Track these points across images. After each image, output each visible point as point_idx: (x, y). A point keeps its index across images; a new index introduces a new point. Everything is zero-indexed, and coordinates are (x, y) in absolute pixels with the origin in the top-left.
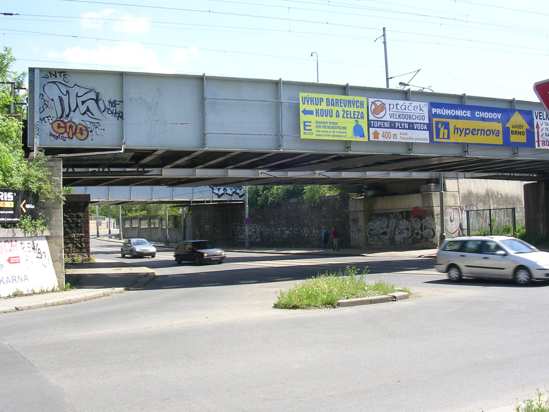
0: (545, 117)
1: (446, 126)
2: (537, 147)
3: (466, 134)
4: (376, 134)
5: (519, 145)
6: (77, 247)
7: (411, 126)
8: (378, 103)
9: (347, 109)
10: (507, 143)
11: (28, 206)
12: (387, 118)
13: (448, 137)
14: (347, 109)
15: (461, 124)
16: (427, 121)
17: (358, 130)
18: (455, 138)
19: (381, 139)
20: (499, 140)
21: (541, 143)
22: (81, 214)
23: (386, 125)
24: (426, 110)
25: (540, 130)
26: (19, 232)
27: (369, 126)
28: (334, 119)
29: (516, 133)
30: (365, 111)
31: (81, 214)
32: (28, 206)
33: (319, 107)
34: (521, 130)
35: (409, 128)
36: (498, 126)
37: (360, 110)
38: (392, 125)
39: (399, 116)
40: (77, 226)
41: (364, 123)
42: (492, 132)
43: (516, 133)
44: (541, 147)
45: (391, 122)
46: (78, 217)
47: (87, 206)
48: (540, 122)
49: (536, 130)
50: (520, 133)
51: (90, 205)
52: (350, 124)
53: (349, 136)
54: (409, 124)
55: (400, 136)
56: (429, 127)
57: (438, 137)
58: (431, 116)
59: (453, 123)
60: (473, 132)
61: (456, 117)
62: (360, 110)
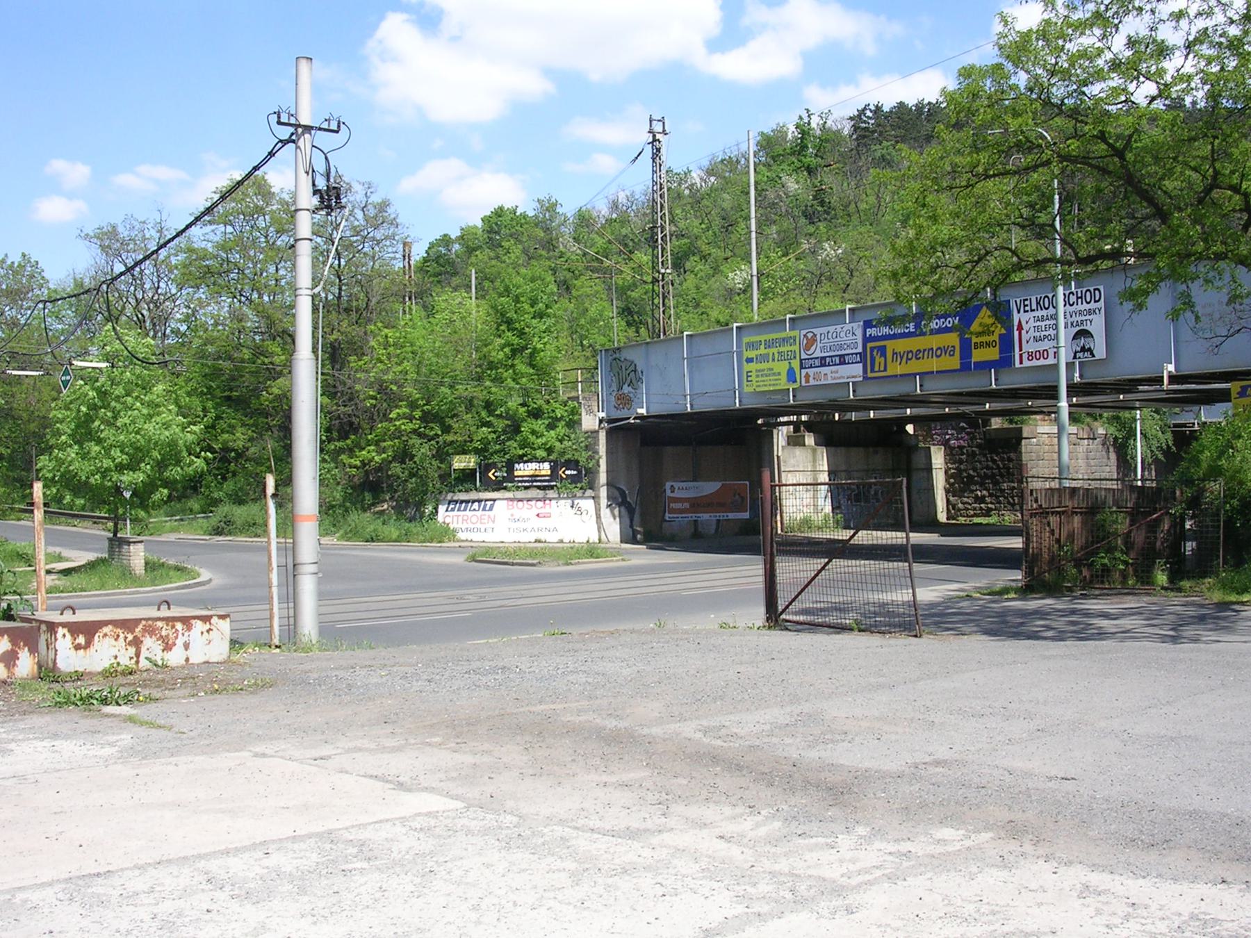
0: (1034, 307)
1: (882, 350)
2: (1017, 365)
3: (908, 359)
4: (807, 376)
5: (985, 366)
6: (1009, 503)
7: (842, 360)
8: (810, 335)
9: (781, 349)
10: (965, 367)
11: (568, 472)
12: (818, 354)
13: (885, 370)
14: (781, 349)
15: (901, 345)
16: (860, 350)
17: (791, 376)
18: (897, 369)
19: (812, 382)
20: (954, 362)
21: (1025, 356)
22: (1012, 455)
23: (817, 363)
24: (859, 333)
25: (1023, 332)
26: (551, 494)
27: (802, 367)
28: (770, 365)
29: (982, 345)
30: (796, 348)
31: (1012, 455)
32: (568, 472)
33: (758, 352)
34: (991, 338)
35: (841, 364)
36: (953, 339)
37: (792, 348)
38: (823, 362)
39: (1038, 303)
40: (1008, 473)
41: (796, 364)
42: (944, 350)
43: (982, 345)
44: (1026, 363)
45: (824, 358)
46: (1010, 460)
47: (1019, 443)
48: (1024, 317)
49: (1016, 333)
50: (988, 344)
51: (1023, 442)
52: (783, 367)
53: (783, 383)
54: (840, 356)
55: (830, 375)
56: (863, 359)
57: (872, 371)
58: (866, 340)
59: (890, 345)
60: (917, 355)
61: (894, 337)
62: (792, 348)
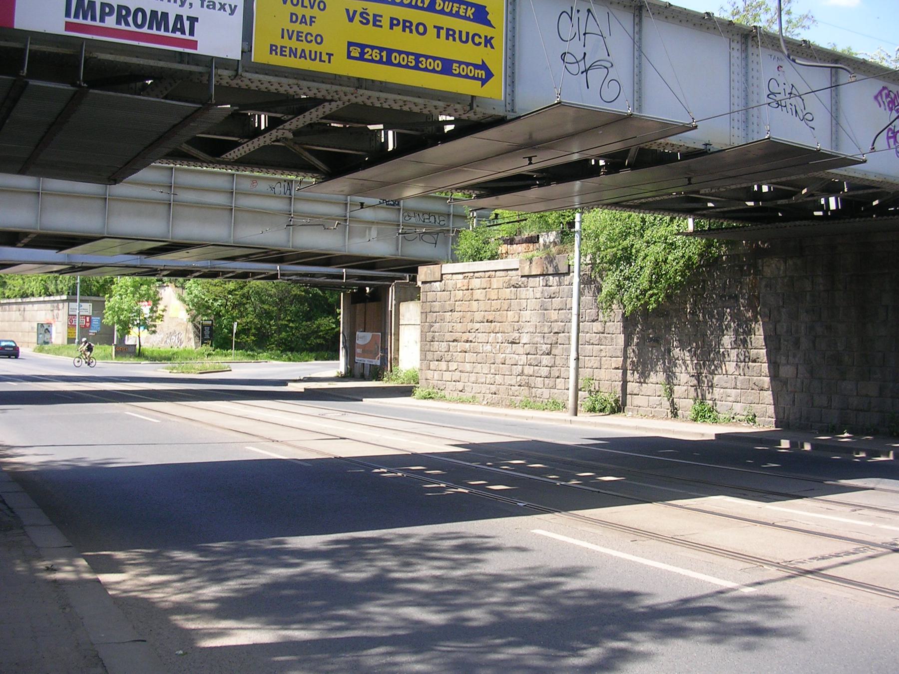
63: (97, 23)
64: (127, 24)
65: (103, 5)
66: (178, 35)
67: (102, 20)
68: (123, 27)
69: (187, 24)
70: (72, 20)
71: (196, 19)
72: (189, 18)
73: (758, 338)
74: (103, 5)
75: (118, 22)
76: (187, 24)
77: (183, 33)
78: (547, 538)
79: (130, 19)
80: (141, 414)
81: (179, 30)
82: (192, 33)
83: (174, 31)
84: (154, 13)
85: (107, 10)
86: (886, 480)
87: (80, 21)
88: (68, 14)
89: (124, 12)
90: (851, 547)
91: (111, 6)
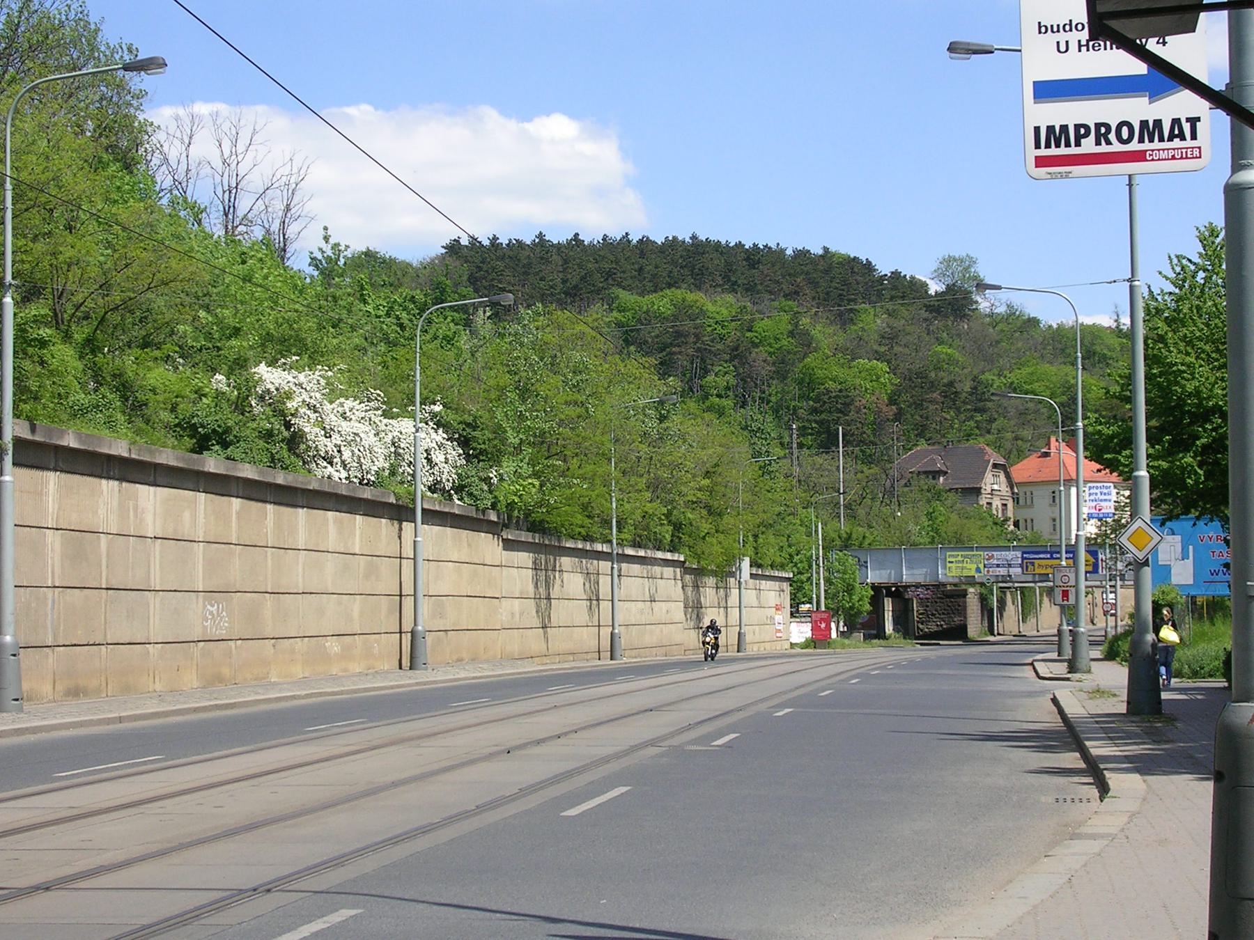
17: (978, 570)
38: (998, 566)
41: (981, 566)
56: (1021, 566)
58: (1023, 558)
63: (1073, 150)
64: (1109, 143)
65: (1077, 127)
66: (1177, 143)
67: (1078, 144)
68: (1104, 148)
69: (1187, 127)
70: (1043, 152)
71: (1198, 119)
72: (1188, 120)
73: (215, 225)
74: (1077, 127)
75: (1098, 143)
76: (1187, 127)
77: (1183, 138)
78: (14, 789)
79: (1112, 137)
80: (145, 763)
81: (1177, 136)
82: (1194, 137)
83: (1170, 139)
84: (1144, 124)
85: (1082, 131)
86: (700, 934)
87: (1053, 151)
88: (1038, 146)
89: (1103, 130)
90: (228, 893)
91: (1087, 127)
